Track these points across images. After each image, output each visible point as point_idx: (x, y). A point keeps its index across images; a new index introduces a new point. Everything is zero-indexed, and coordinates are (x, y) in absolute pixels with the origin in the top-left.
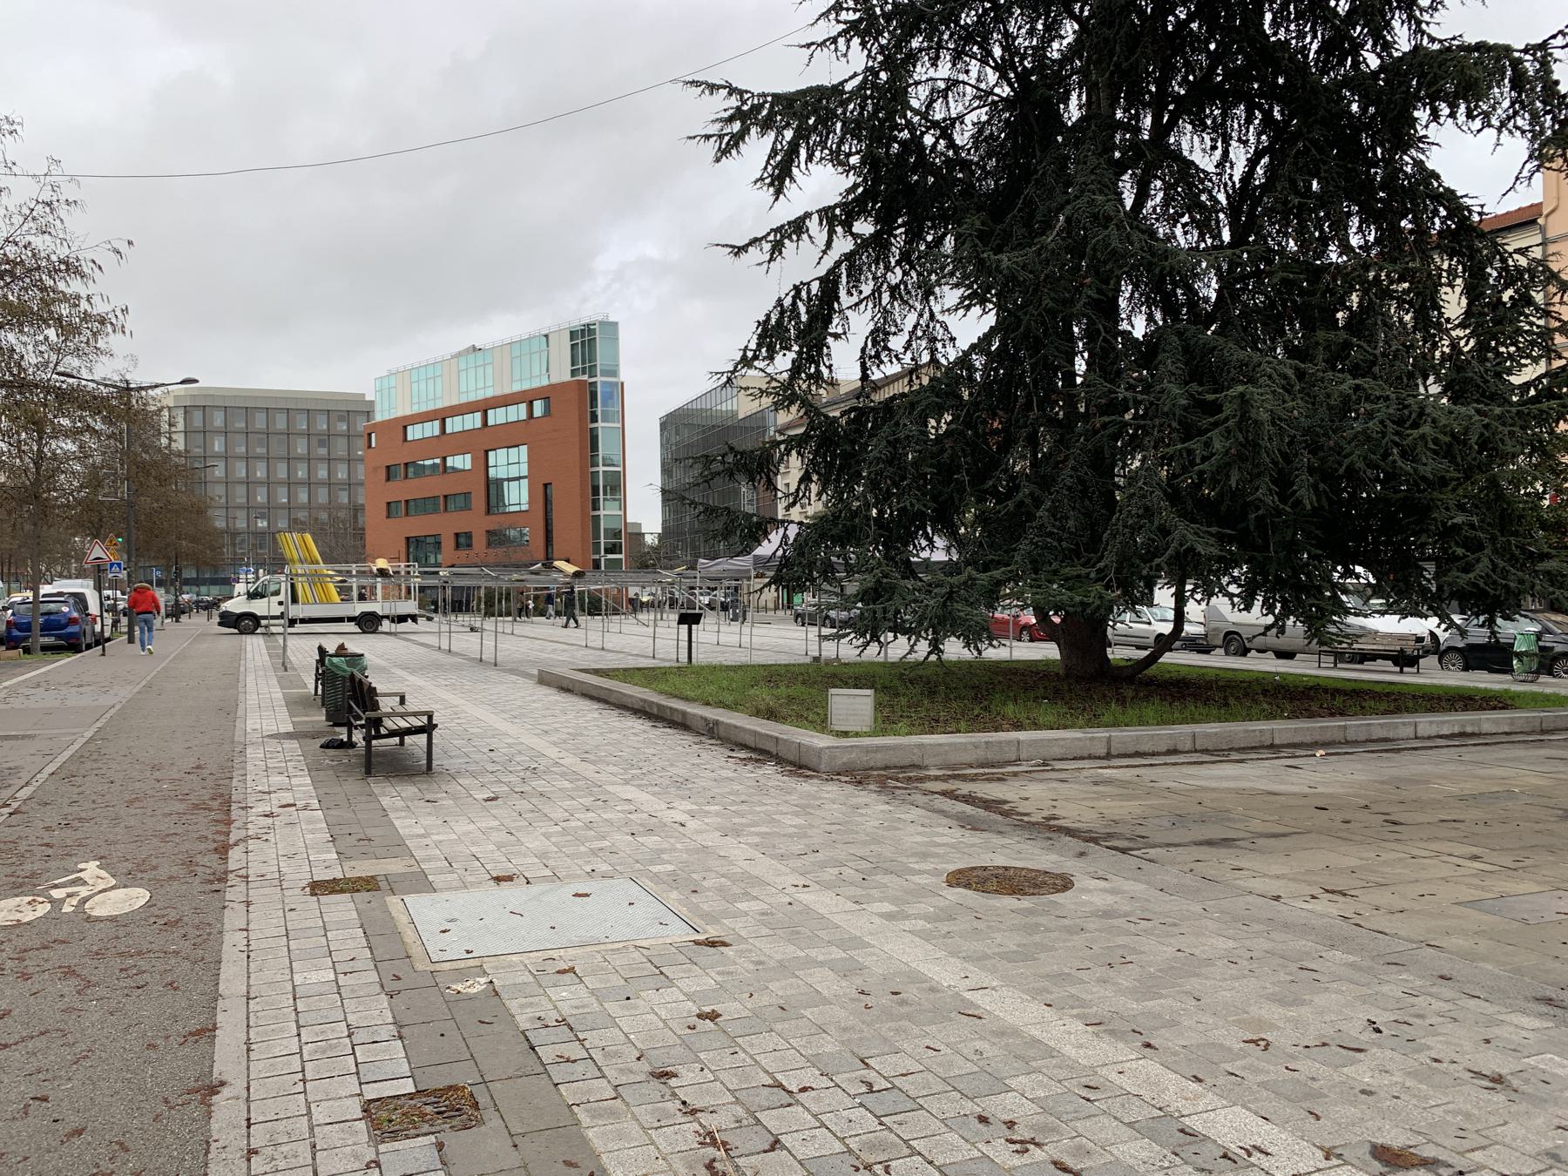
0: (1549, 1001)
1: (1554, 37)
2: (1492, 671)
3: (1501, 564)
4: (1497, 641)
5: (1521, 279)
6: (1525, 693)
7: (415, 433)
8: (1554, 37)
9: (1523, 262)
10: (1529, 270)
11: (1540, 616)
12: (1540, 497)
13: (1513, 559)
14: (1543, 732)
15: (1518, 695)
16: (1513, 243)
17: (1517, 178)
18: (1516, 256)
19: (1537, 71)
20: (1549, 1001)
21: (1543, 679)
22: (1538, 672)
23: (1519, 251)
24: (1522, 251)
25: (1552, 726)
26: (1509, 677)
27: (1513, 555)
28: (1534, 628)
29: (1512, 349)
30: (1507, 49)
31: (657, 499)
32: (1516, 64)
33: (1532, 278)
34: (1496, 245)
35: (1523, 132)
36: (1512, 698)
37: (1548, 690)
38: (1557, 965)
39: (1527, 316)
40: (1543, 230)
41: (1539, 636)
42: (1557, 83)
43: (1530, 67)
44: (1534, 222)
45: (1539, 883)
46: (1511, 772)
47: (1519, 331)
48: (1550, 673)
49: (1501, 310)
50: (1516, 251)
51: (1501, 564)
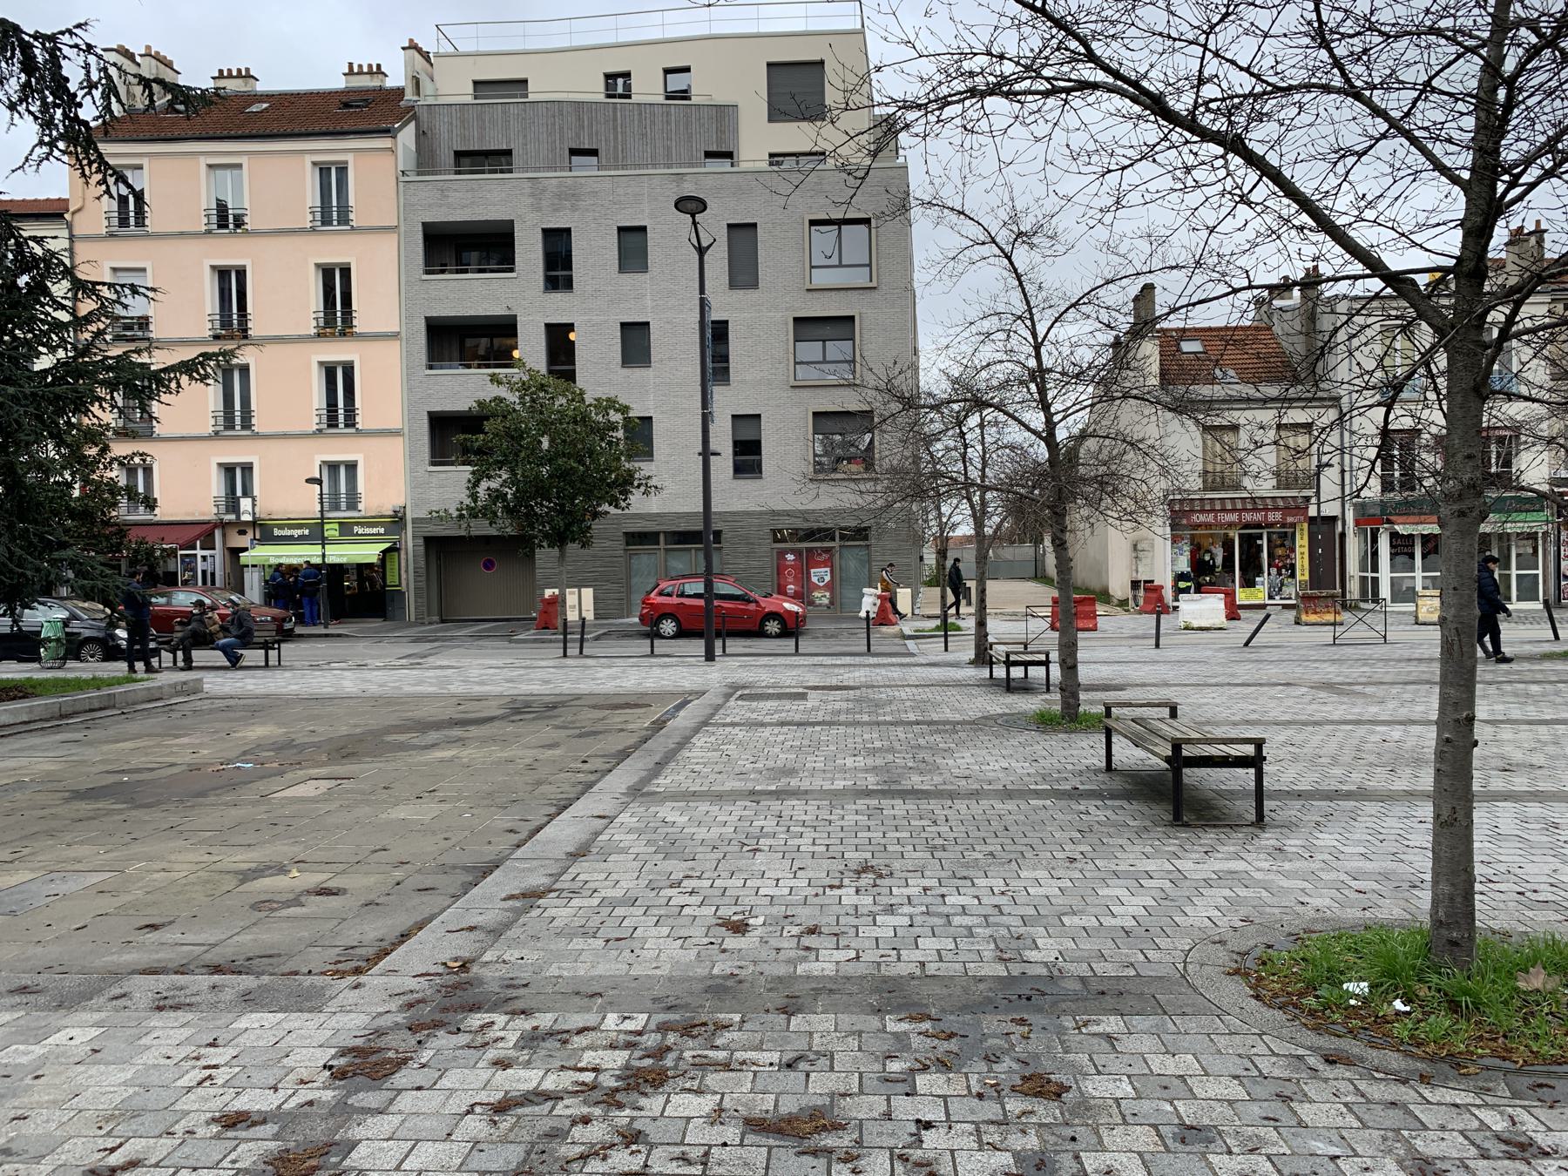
0: (23, 990)
1: (62, 33)
2: (21, 660)
3: (18, 551)
4: (20, 628)
5: (38, 268)
6: (47, 680)
7: (1187, 347)
8: (62, 33)
9: (38, 251)
10: (44, 260)
11: (69, 604)
12: (69, 486)
13: (29, 547)
14: (62, 717)
15: (42, 683)
16: (29, 230)
17: (27, 159)
18: (31, 243)
19: (46, 61)
20: (23, 990)
21: (70, 664)
22: (64, 659)
23: (34, 239)
24: (39, 240)
25: (70, 710)
26: (36, 665)
27: (31, 543)
28: (63, 615)
29: (30, 336)
30: (17, 29)
31: (730, 443)
32: (26, 48)
33: (48, 267)
34: (10, 227)
35: (36, 118)
36: (33, 687)
37: (70, 675)
38: (39, 949)
39: (43, 305)
40: (70, 226)
41: (66, 623)
42: (67, 80)
43: (40, 56)
44: (61, 216)
45: (32, 870)
46: (24, 762)
47: (34, 319)
48: (78, 658)
49: (15, 296)
50: (30, 238)
51: (18, 551)
